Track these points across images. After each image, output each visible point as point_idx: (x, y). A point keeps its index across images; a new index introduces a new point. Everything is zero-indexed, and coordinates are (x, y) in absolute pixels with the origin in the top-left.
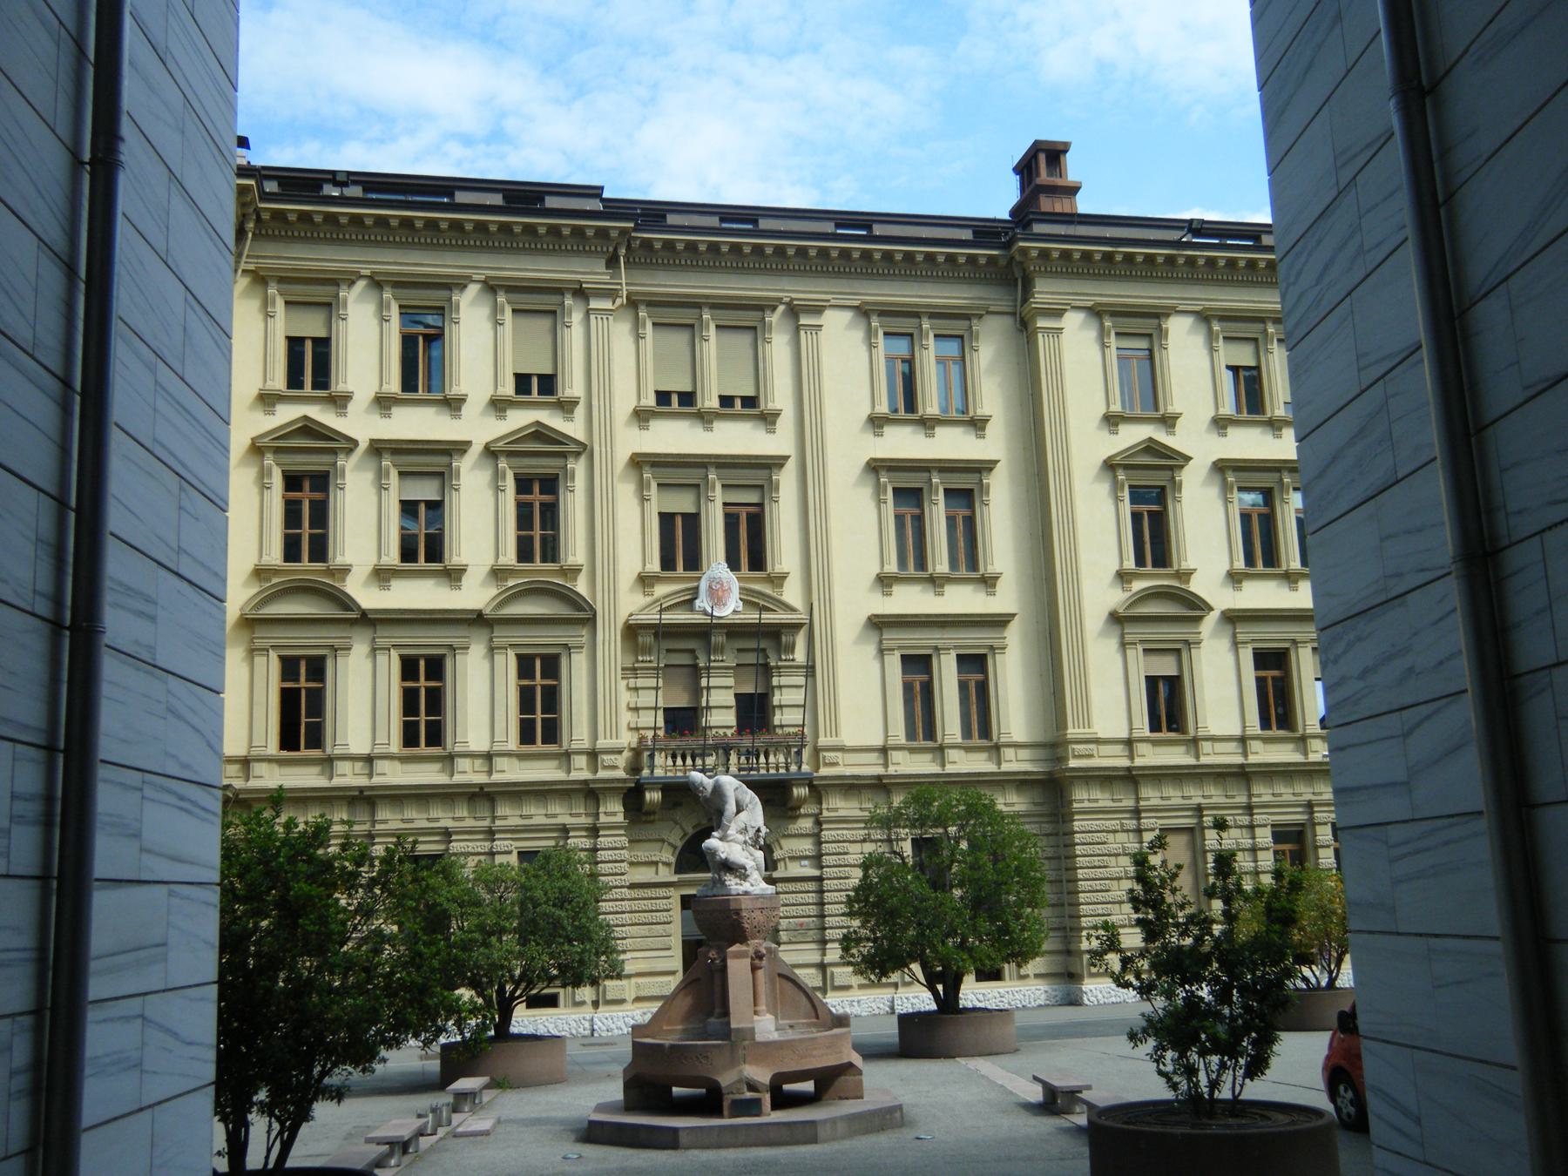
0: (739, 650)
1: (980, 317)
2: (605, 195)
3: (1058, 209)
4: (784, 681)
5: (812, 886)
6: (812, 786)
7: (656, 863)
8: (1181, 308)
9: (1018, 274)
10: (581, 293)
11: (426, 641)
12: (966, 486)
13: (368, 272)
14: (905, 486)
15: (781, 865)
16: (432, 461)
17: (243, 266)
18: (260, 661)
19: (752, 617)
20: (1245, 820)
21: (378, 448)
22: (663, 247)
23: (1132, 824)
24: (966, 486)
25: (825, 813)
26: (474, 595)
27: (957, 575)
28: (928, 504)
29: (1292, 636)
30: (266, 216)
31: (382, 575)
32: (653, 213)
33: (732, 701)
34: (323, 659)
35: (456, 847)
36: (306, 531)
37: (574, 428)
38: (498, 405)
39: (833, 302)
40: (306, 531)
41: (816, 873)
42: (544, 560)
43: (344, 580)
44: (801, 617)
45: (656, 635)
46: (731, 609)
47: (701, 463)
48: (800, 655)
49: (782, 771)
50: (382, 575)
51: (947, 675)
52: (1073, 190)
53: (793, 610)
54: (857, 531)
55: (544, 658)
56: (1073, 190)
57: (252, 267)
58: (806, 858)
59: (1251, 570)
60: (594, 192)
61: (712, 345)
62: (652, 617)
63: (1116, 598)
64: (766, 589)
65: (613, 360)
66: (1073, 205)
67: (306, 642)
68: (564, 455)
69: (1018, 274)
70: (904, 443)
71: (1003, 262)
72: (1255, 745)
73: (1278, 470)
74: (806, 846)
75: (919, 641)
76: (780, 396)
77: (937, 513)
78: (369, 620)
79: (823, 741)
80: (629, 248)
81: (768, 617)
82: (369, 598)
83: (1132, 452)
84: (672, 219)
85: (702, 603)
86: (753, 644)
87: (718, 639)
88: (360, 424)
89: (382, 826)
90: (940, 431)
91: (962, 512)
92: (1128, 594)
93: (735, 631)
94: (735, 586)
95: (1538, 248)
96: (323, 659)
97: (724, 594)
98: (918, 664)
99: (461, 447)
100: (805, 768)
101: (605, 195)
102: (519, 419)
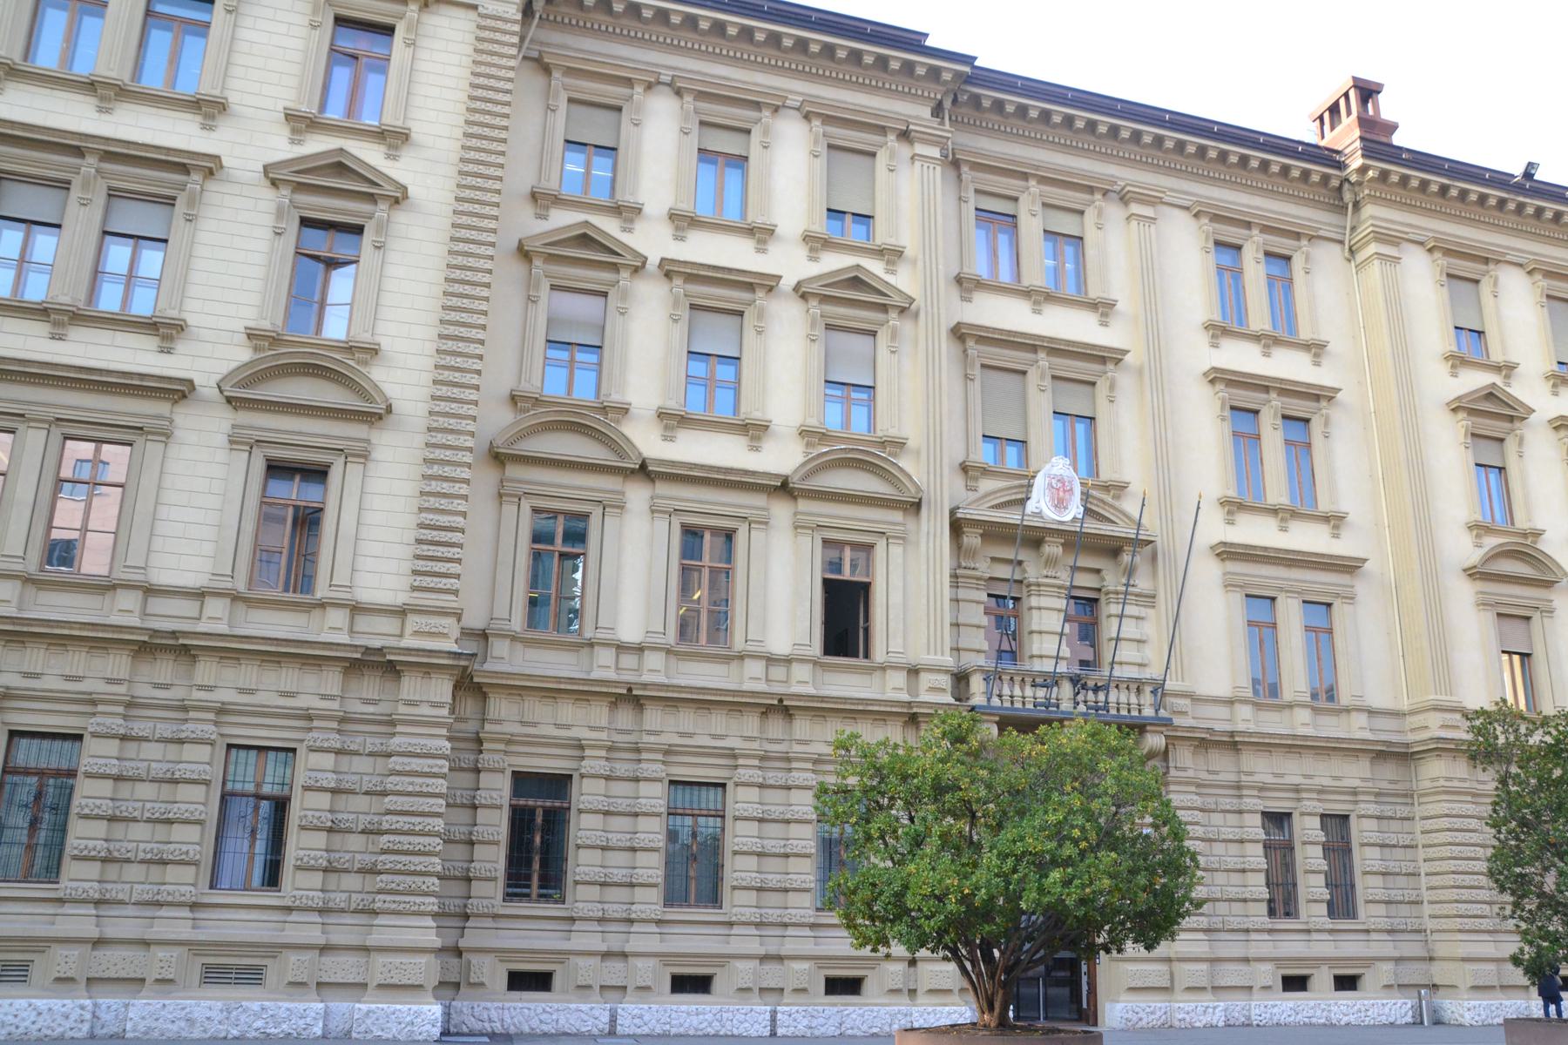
0: (994, 559)
2: (977, 63)
8: (1508, 258)
9: (1348, 197)
10: (905, 135)
12: (1304, 409)
13: (667, 79)
14: (1243, 399)
16: (722, 298)
21: (669, 270)
22: (655, 15)
24: (1304, 409)
25: (1173, 772)
28: (1274, 416)
31: (673, 421)
33: (811, 847)
37: (903, 280)
38: (816, 243)
39: (1411, 237)
47: (1030, 345)
49: (1135, 713)
50: (673, 421)
52: (1392, 128)
56: (1392, 128)
60: (969, 60)
70: (1243, 358)
77: (1273, 437)
78: (644, 471)
80: (955, 101)
82: (648, 442)
87: (1052, 548)
89: (652, 739)
93: (1075, 541)
95: (23, 147)
96: (585, 517)
99: (767, 284)
101: (977, 63)
102: (834, 262)
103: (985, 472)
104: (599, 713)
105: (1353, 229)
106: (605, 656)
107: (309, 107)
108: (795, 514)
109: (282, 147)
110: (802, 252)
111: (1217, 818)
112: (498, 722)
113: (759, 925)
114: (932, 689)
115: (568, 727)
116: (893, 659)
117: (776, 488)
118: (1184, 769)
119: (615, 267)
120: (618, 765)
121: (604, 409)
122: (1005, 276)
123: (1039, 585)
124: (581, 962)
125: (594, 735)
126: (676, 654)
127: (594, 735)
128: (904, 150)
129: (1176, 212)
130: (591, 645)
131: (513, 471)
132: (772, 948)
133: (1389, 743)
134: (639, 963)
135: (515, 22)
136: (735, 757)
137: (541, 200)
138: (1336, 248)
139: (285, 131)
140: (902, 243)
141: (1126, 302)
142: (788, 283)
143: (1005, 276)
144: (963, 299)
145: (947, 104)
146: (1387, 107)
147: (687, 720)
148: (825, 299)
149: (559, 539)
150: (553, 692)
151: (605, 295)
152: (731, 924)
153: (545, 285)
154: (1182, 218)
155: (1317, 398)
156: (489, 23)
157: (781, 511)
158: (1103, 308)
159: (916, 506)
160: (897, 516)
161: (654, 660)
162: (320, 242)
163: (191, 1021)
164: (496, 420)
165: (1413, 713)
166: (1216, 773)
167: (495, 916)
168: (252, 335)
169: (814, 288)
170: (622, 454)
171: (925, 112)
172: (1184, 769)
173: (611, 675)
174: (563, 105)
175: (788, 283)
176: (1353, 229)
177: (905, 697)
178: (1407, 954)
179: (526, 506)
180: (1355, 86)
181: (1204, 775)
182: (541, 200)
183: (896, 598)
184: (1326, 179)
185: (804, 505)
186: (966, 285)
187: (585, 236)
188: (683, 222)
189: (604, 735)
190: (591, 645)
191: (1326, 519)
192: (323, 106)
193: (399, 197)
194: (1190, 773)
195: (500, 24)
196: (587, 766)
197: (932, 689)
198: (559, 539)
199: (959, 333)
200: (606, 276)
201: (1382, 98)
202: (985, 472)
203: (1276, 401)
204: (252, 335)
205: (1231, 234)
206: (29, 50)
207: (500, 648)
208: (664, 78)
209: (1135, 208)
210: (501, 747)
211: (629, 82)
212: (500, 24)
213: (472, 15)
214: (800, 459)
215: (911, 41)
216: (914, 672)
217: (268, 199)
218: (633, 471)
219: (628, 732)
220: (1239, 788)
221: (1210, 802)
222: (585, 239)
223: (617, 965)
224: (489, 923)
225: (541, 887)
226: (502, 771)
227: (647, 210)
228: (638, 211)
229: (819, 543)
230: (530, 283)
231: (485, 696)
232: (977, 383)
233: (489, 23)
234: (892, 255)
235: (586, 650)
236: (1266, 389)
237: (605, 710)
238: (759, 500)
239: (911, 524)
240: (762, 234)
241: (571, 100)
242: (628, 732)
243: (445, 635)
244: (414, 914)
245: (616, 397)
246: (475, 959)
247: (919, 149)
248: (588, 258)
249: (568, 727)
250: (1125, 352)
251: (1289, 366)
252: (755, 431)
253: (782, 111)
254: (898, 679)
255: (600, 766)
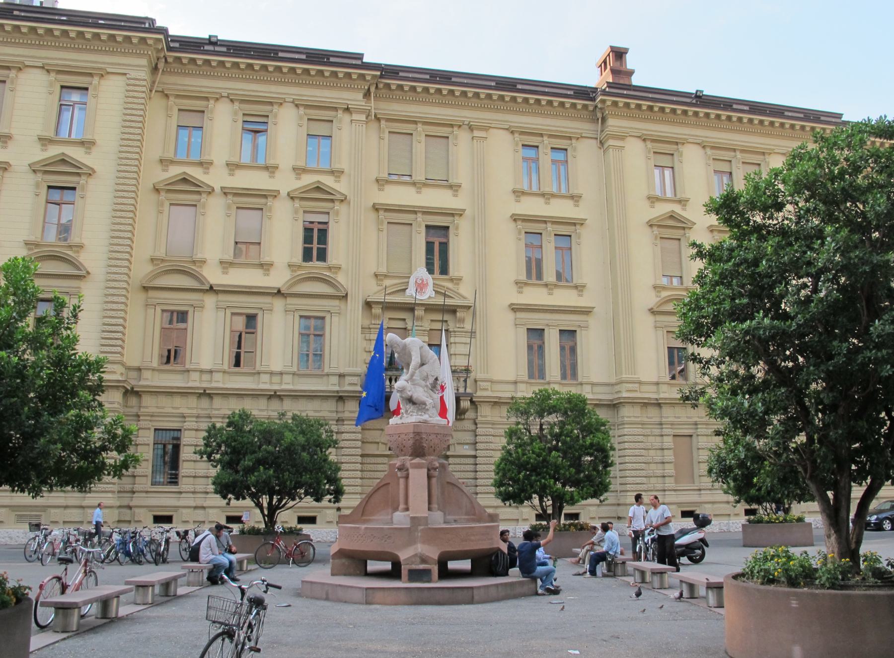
0: (432, 321)
1: (683, 144)
3: (622, 82)
4: (457, 340)
5: (471, 461)
6: (472, 402)
7: (378, 443)
9: (599, 115)
10: (347, 110)
11: (250, 303)
12: (567, 232)
13: (226, 95)
14: (531, 228)
15: (452, 448)
16: (253, 200)
17: (155, 88)
18: (151, 311)
19: (440, 300)
20: (657, 431)
21: (225, 192)
23: (657, 431)
24: (567, 232)
25: (479, 418)
26: (278, 279)
27: (530, 282)
28: (547, 244)
29: (327, 309)
30: (170, 60)
31: (226, 265)
32: (390, 72)
34: (186, 313)
35: (187, 425)
36: (315, 246)
37: (341, 186)
40: (315, 246)
41: (473, 453)
42: (318, 260)
43: (201, 267)
44: (469, 302)
45: (426, 310)
46: (428, 295)
48: (468, 326)
50: (226, 265)
51: (552, 341)
52: (631, 73)
53: (465, 298)
54: (507, 254)
55: (178, 312)
56: (631, 73)
57: (160, 89)
58: (467, 444)
59: (530, 282)
61: (420, 146)
62: (380, 298)
63: (652, 299)
64: (449, 285)
65: (358, 149)
66: (630, 80)
67: (178, 301)
68: (332, 201)
69: (599, 115)
70: (533, 207)
71: (591, 108)
72: (664, 388)
73: (545, 222)
74: (469, 437)
75: (537, 320)
76: (462, 174)
79: (480, 376)
80: (377, 87)
81: (449, 302)
82: (214, 276)
83: (662, 218)
84: (453, 79)
85: (411, 291)
86: (439, 317)
87: (419, 312)
88: (217, 178)
89: (217, 412)
90: (553, 201)
91: (437, 241)
92: (658, 299)
93: (430, 308)
94: (431, 282)
96: (186, 313)
97: (422, 286)
98: (536, 334)
99: (274, 194)
100: (469, 390)
103: (664, 288)
104: (193, 401)
105: (602, 131)
106: (195, 376)
107: (51, 134)
108: (148, 298)
109: (39, 155)
110: (293, 176)
111: (651, 439)
112: (146, 407)
113: (194, 493)
114: (350, 384)
115: (178, 408)
116: (332, 371)
117: (276, 294)
118: (486, 416)
119: (199, 193)
120: (201, 424)
121: (194, 262)
122: (669, 194)
123: (455, 332)
124: (184, 511)
125: (190, 411)
126: (228, 373)
127: (190, 411)
128: (346, 118)
129: (501, 131)
130: (259, 373)
131: (152, 294)
132: (199, 503)
133: (600, 400)
134: (211, 511)
135: (145, 80)
136: (184, 417)
137: (165, 162)
138: (594, 141)
139: (38, 146)
140: (343, 167)
141: (466, 185)
142: (284, 193)
143: (669, 194)
144: (380, 190)
145: (373, 89)
146: (630, 62)
147: (164, 401)
148: (302, 199)
149: (312, 329)
150: (170, 393)
151: (195, 206)
152: (181, 493)
153: (167, 204)
154: (505, 136)
155: (453, 215)
156: (132, 82)
157: (278, 304)
158: (455, 188)
159: (345, 297)
160: (336, 302)
161: (287, 378)
162: (56, 195)
163: (11, 538)
164: (141, 270)
165: (617, 384)
166: (679, 417)
167: (147, 492)
168: (27, 244)
169: (296, 194)
170: (203, 284)
171: (360, 96)
172: (486, 416)
173: (197, 384)
174: (387, 135)
175: (284, 193)
176: (602, 131)
177: (337, 388)
178: (70, 504)
179: (159, 309)
180: (612, 51)
181: (646, 419)
182: (653, 200)
183: (335, 342)
184: (585, 107)
185: (290, 300)
186: (519, 194)
187: (184, 179)
188: (233, 167)
189: (194, 411)
190: (259, 373)
191: (576, 287)
192: (57, 132)
193: (91, 173)
194: (489, 419)
195: (137, 83)
196: (187, 425)
197: (350, 384)
198: (312, 329)
199: (376, 208)
200: (196, 197)
201: (628, 57)
202: (664, 288)
203: (550, 227)
204: (27, 244)
205: (533, 141)
206: (57, 132)
207: (146, 374)
208: (224, 94)
209: (476, 133)
210: (149, 418)
211: (207, 99)
212: (137, 83)
213: (124, 78)
214: (289, 277)
215: (353, 61)
216: (341, 376)
217: (31, 178)
218: (207, 290)
219: (206, 409)
220: (661, 424)
221: (648, 432)
222: (184, 181)
223: (201, 512)
224: (144, 495)
225: (38, 477)
226: (149, 429)
227: (215, 162)
228: (211, 163)
229: (297, 318)
230: (160, 204)
231: (140, 396)
232: (385, 232)
233: (132, 82)
234: (336, 173)
235: (186, 374)
236: (415, 212)
237: (195, 400)
238: (268, 299)
239: (343, 306)
240: (271, 169)
241: (390, 132)
242: (206, 409)
243: (114, 372)
244: (103, 492)
245: (199, 256)
246: (137, 510)
247: (355, 117)
248: (186, 189)
249: (178, 408)
250: (464, 210)
251: (561, 209)
252: (266, 267)
253: (285, 104)
254: (335, 380)
255: (194, 425)
